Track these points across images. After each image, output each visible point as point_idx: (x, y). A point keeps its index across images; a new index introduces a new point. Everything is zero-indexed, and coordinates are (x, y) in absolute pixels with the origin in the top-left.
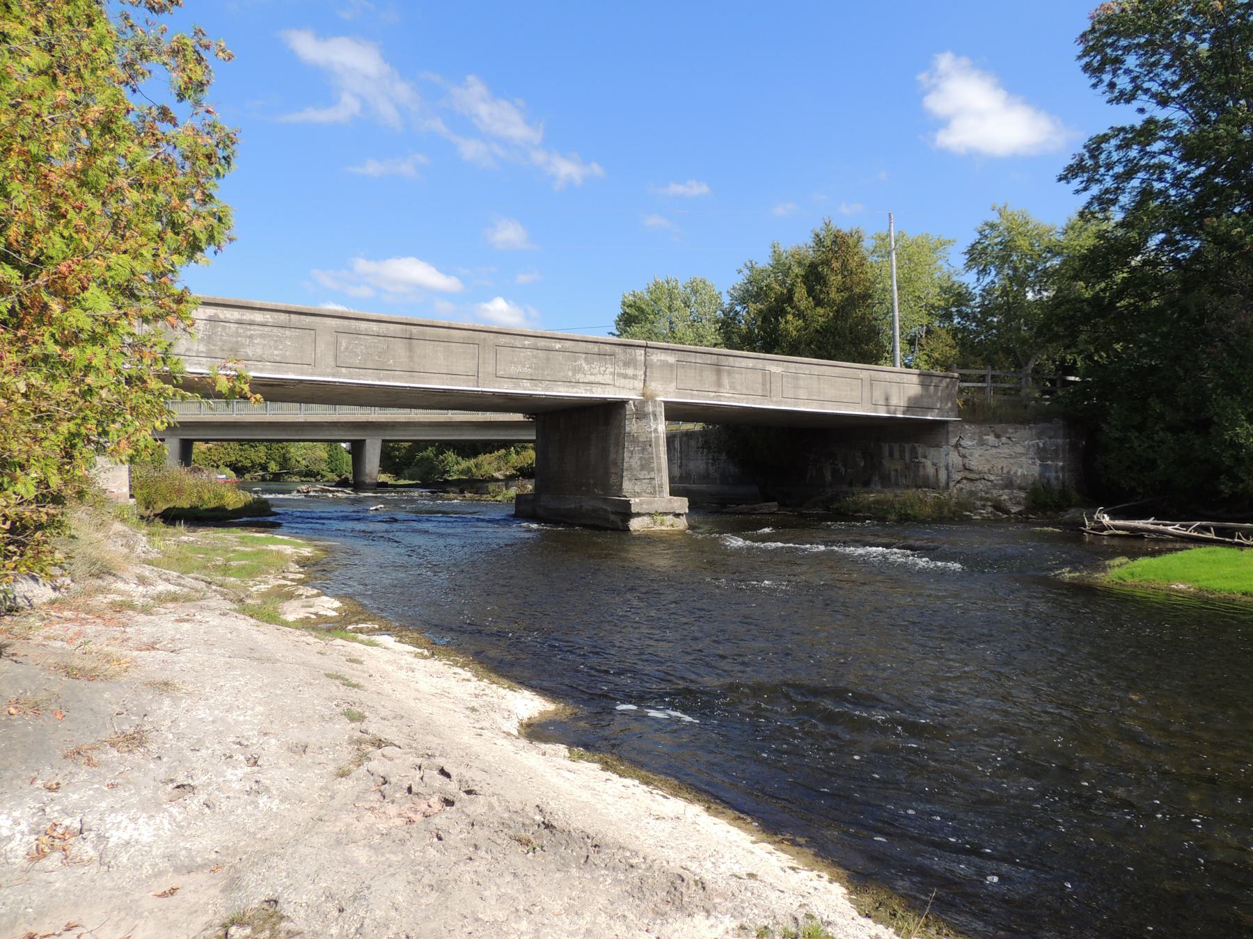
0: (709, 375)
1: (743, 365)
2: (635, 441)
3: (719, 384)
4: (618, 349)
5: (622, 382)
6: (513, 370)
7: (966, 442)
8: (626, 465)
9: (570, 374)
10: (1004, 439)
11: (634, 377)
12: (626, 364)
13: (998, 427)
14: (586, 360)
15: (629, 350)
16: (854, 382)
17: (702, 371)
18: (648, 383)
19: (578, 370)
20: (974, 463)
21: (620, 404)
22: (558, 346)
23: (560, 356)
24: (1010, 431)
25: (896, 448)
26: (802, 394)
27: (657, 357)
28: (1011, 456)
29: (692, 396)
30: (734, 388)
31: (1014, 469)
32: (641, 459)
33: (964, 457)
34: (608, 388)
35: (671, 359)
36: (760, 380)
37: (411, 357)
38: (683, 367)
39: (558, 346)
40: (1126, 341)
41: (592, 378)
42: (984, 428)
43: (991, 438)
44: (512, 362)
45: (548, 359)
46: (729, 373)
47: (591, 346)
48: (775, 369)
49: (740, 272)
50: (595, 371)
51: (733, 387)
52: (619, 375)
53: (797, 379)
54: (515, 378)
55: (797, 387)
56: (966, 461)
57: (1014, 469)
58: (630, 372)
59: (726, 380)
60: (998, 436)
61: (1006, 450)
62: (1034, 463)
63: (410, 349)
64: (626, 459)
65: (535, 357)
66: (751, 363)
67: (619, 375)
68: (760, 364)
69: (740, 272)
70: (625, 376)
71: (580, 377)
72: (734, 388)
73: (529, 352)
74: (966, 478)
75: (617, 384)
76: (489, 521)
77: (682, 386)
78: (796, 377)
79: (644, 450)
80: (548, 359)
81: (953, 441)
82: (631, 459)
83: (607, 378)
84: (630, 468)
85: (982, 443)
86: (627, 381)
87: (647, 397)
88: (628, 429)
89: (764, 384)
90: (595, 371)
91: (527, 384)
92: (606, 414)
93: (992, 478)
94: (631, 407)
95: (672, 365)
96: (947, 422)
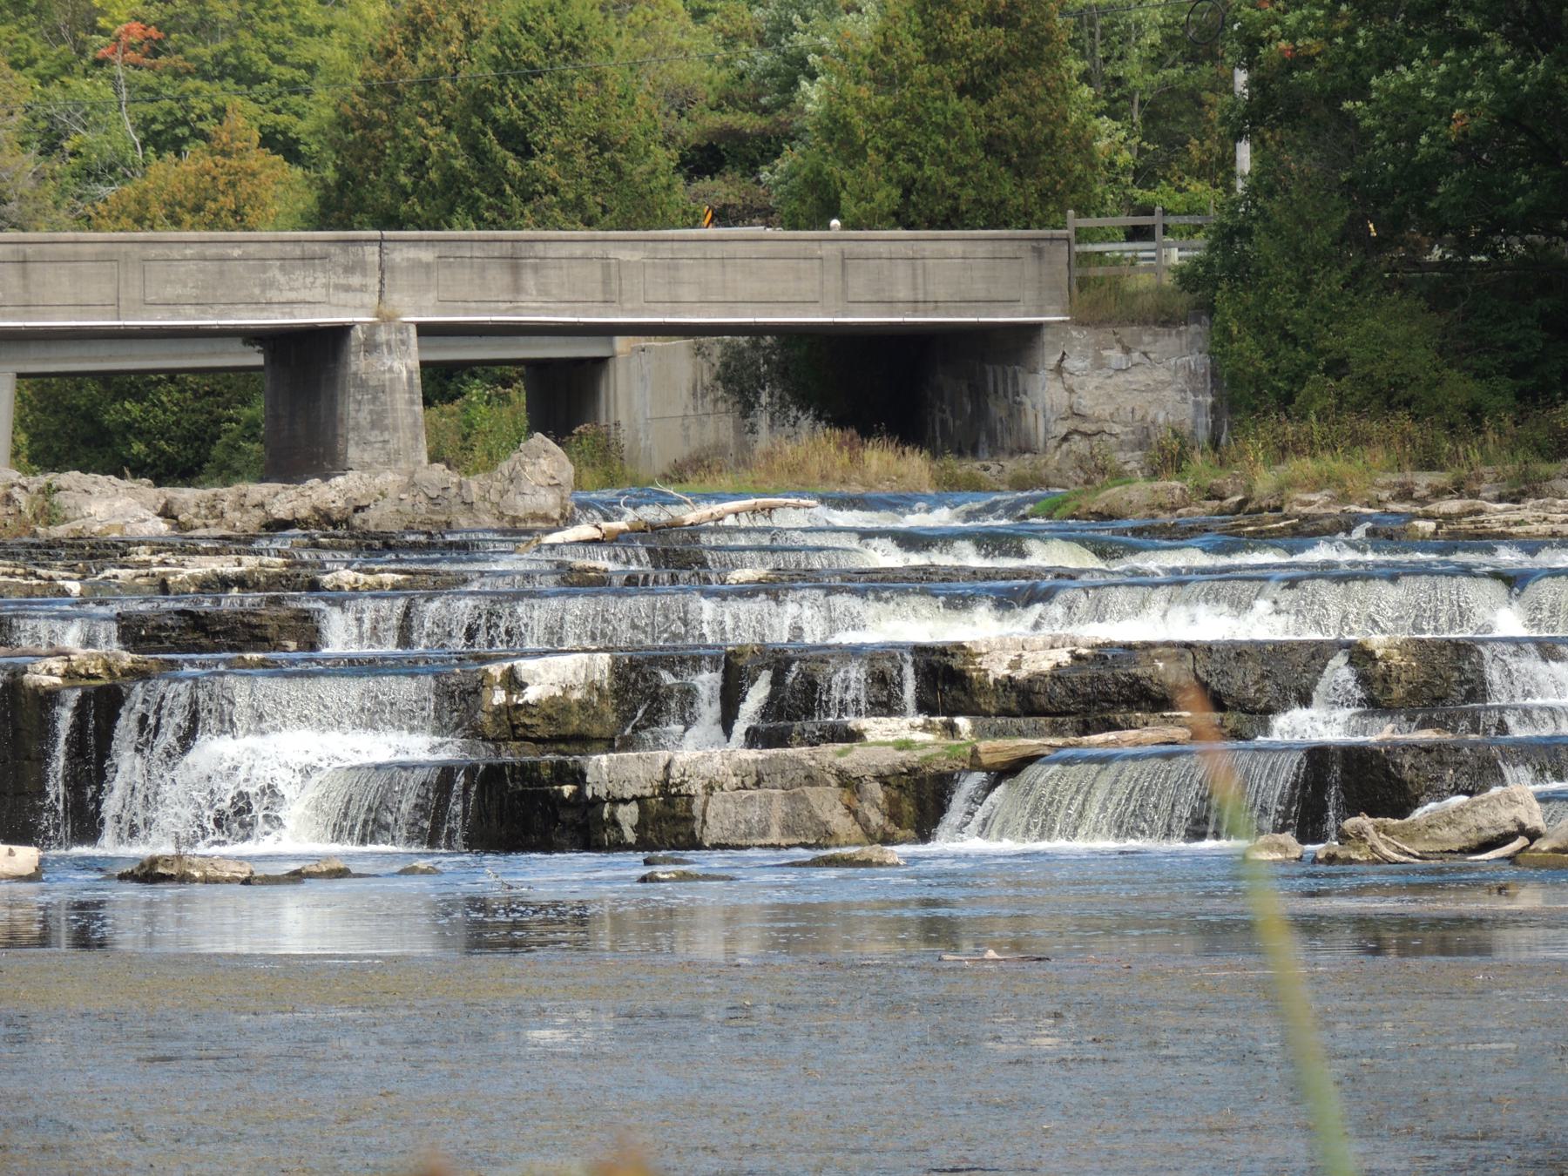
0: (498, 278)
1: (564, 253)
2: (363, 385)
3: (517, 288)
4: (333, 249)
5: (343, 297)
6: (170, 292)
7: (1072, 363)
8: (351, 422)
9: (257, 291)
10: (1136, 356)
11: (363, 289)
12: (349, 270)
13: (1127, 332)
14: (282, 268)
15: (352, 249)
16: (803, 264)
17: (483, 269)
18: (386, 296)
19: (266, 285)
20: (1086, 403)
21: (340, 333)
22: (236, 252)
23: (240, 267)
24: (1146, 339)
25: (999, 369)
26: (686, 293)
28: (1148, 388)
29: (467, 312)
30: (547, 293)
31: (1152, 412)
32: (371, 412)
33: (1071, 390)
34: (297, 309)
35: (427, 255)
36: (598, 274)
37: (26, 287)
38: (450, 265)
39: (236, 252)
40: (1424, 129)
41: (292, 296)
42: (1105, 334)
43: (1115, 355)
44: (168, 281)
45: (221, 273)
46: (536, 269)
47: (288, 247)
48: (625, 254)
50: (296, 284)
51: (543, 291)
52: (337, 287)
53: (676, 268)
54: (172, 304)
56: (1074, 398)
57: (1152, 412)
58: (356, 280)
59: (529, 281)
60: (1127, 351)
61: (1140, 377)
62: (1184, 400)
63: (25, 275)
64: (353, 414)
65: (201, 271)
67: (337, 287)
68: (597, 250)
70: (348, 289)
71: (273, 295)
72: (547, 293)
73: (192, 265)
74: (1076, 431)
75: (334, 300)
76: (793, 865)
77: (447, 296)
78: (673, 265)
79: (375, 399)
80: (221, 273)
81: (1052, 360)
83: (318, 294)
84: (357, 428)
85: (1099, 364)
86: (350, 295)
87: (387, 319)
88: (354, 368)
89: (606, 282)
90: (296, 284)
91: (190, 310)
92: (325, 345)
93: (1117, 429)
94: (358, 334)
95: (428, 266)
96: (1038, 327)
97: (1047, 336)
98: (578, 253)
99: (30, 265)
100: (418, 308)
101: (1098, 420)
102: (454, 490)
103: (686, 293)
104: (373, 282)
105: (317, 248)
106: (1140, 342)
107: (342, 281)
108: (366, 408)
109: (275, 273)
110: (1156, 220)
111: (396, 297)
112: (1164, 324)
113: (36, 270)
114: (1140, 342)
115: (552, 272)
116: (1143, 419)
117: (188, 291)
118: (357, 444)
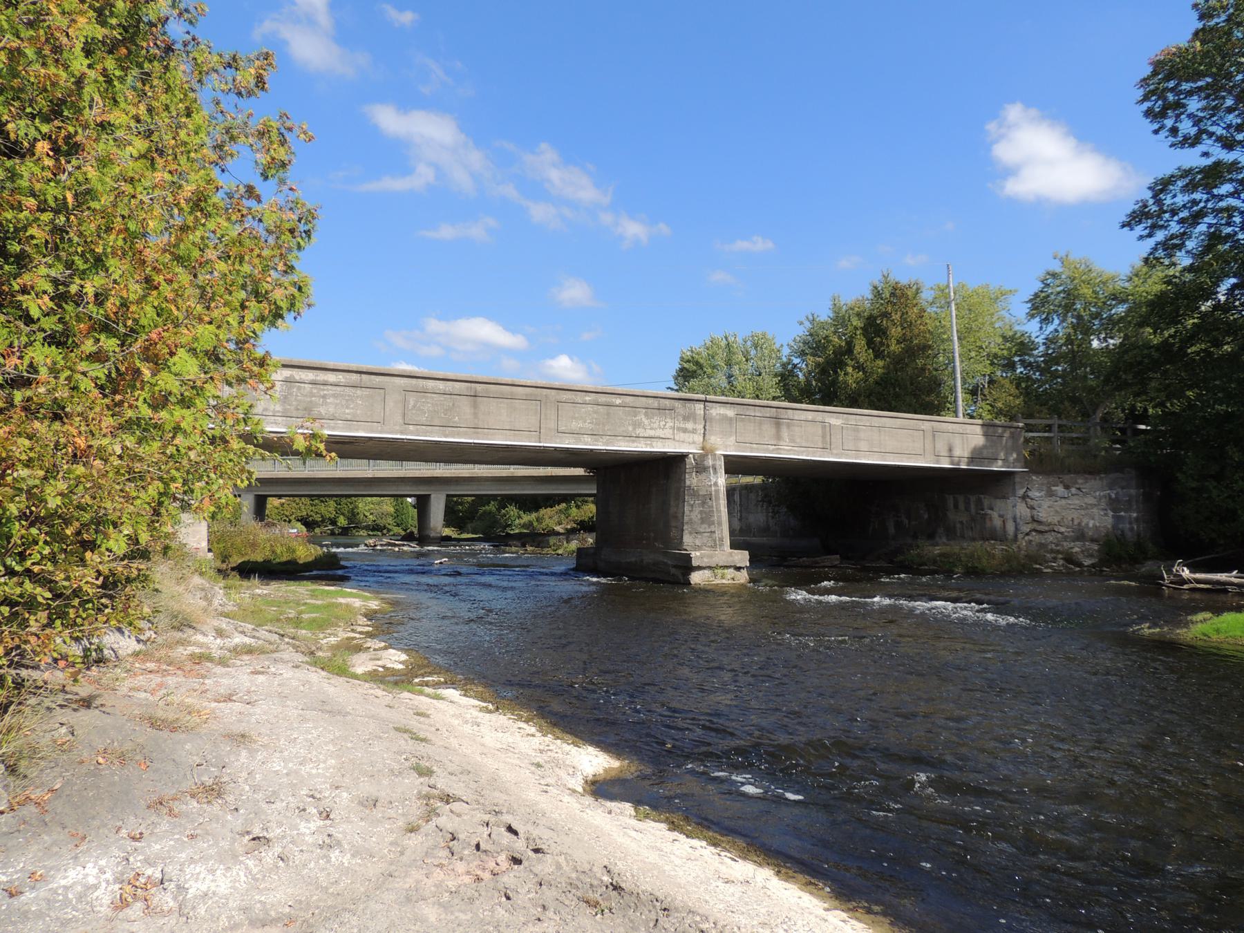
0: (769, 429)
1: (803, 418)
2: (695, 494)
3: (778, 437)
4: (677, 404)
5: (681, 436)
6: (575, 425)
9: (630, 428)
10: (1073, 490)
11: (694, 431)
12: (686, 418)
14: (646, 414)
15: (688, 405)
16: (916, 433)
17: (760, 424)
20: (1042, 515)
21: (680, 458)
22: (618, 401)
23: (620, 411)
25: (961, 499)
26: (863, 446)
27: (717, 411)
28: (1081, 508)
31: (1085, 521)
32: (701, 512)
33: (1032, 508)
35: (730, 412)
37: (475, 415)
38: (743, 420)
41: (652, 433)
43: (1060, 489)
44: (574, 418)
45: (608, 414)
46: (788, 426)
47: (650, 401)
49: (801, 323)
50: (656, 426)
51: (792, 440)
52: (679, 429)
55: (857, 439)
56: (1035, 512)
57: (1085, 521)
58: (690, 426)
59: (785, 433)
60: (1067, 487)
61: (1076, 501)
62: (1106, 515)
63: (475, 406)
64: (687, 512)
65: (595, 412)
66: (810, 416)
67: (679, 429)
68: (819, 417)
69: (801, 323)
70: (685, 431)
71: (640, 432)
73: (589, 408)
75: (677, 438)
78: (856, 428)
79: (704, 503)
80: (608, 414)
82: (692, 512)
83: (667, 433)
84: (691, 522)
85: (1051, 494)
87: (707, 451)
88: (688, 483)
89: (824, 437)
90: (656, 426)
91: (588, 439)
93: (1062, 529)
94: (691, 461)
95: (731, 419)
97: (1017, 479)
98: (810, 418)
99: (479, 399)
100: (727, 445)
101: (1050, 524)
102: (50, 61)
103: (863, 446)
104: (700, 427)
105: (667, 402)
106: (1076, 483)
107: (682, 425)
108: (697, 510)
109: (641, 417)
110: (361, 548)
111: (713, 438)
112: (1090, 473)
113: (484, 403)
114: (1076, 483)
115: (796, 429)
116: (1079, 524)
117: (587, 425)
118: (691, 533)
